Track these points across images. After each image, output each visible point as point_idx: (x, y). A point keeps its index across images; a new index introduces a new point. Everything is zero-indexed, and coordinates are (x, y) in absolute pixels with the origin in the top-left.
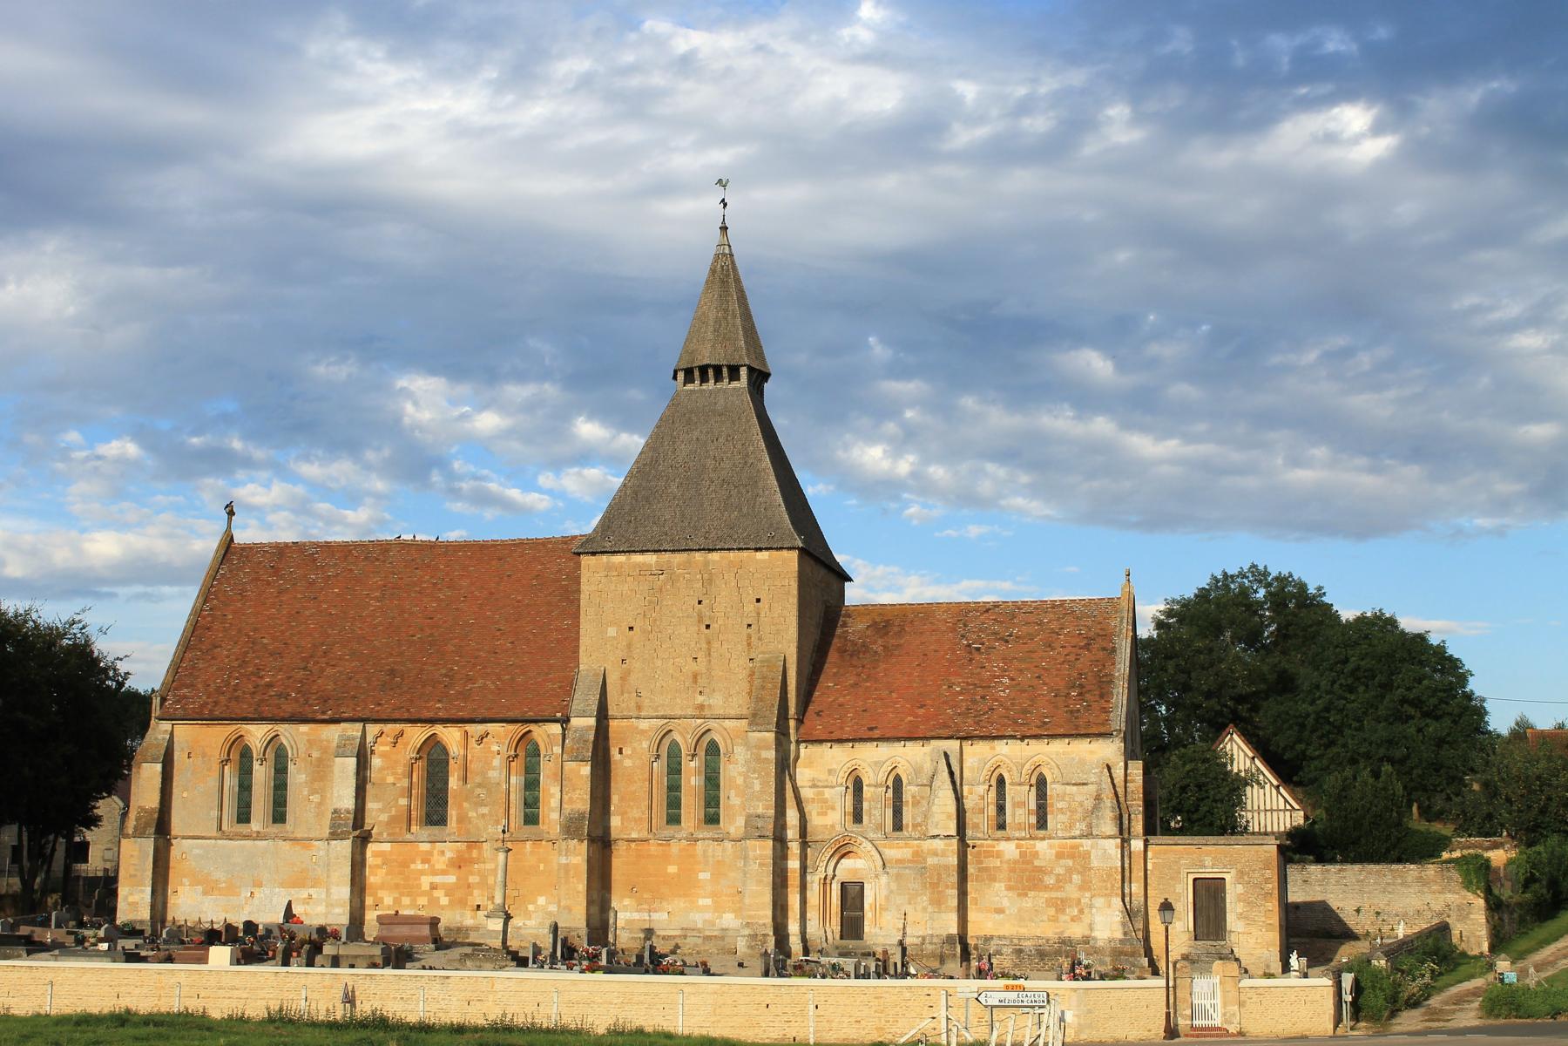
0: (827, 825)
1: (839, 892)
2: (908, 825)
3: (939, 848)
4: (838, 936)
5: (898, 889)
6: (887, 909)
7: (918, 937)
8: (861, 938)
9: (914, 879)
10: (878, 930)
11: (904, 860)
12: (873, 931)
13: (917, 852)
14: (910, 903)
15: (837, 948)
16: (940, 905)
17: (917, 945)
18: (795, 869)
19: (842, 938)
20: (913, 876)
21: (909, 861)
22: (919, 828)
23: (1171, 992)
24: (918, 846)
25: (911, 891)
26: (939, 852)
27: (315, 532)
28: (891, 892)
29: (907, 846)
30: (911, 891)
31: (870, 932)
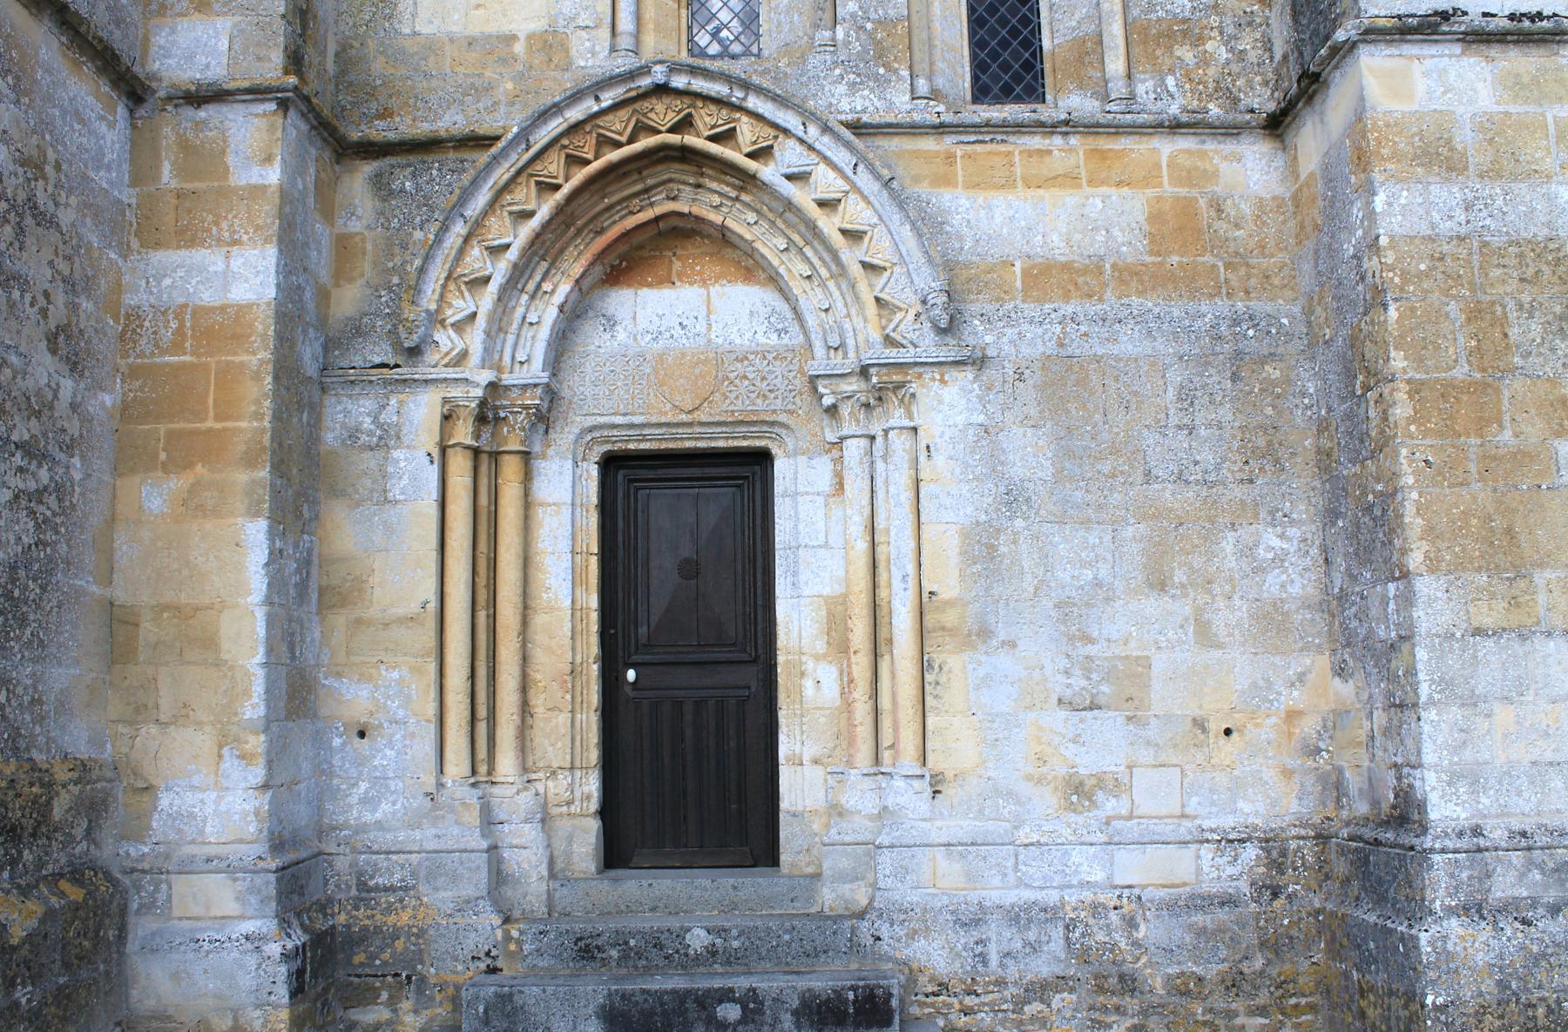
0: (511, 38)
1: (593, 520)
2: (1090, 49)
3: (1463, 111)
4: (585, 838)
5: (1059, 476)
6: (985, 633)
7: (1231, 842)
8: (766, 852)
9: (1186, 398)
10: (907, 796)
11: (1095, 268)
12: (860, 797)
13: (1186, 208)
14: (1160, 584)
15: (587, 951)
16: (1520, 573)
17: (1228, 901)
18: (243, 310)
19: (614, 855)
20: (1175, 376)
21: (1129, 276)
22: (1186, 54)
23: (482, 712)
24: (1188, 177)
25: (1167, 494)
26: (1465, 137)
27: (707, 883)
28: (1013, 499)
29: (1102, 172)
30: (1167, 494)
31: (837, 811)
